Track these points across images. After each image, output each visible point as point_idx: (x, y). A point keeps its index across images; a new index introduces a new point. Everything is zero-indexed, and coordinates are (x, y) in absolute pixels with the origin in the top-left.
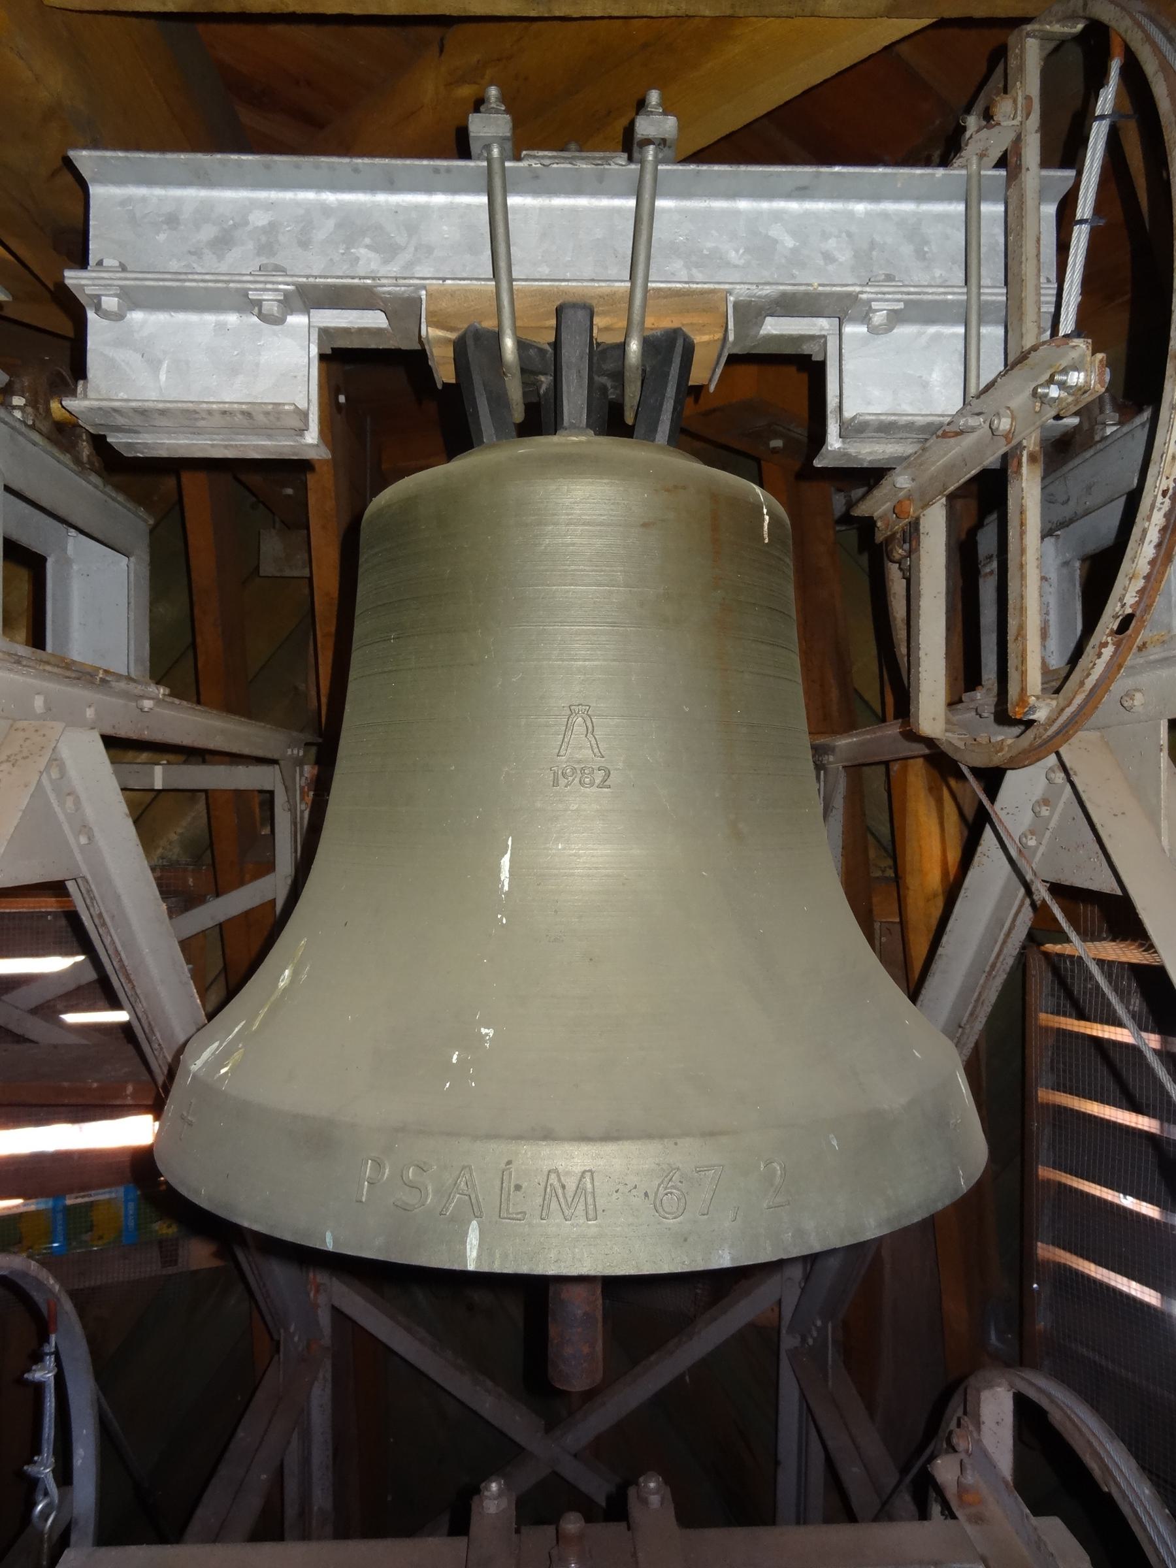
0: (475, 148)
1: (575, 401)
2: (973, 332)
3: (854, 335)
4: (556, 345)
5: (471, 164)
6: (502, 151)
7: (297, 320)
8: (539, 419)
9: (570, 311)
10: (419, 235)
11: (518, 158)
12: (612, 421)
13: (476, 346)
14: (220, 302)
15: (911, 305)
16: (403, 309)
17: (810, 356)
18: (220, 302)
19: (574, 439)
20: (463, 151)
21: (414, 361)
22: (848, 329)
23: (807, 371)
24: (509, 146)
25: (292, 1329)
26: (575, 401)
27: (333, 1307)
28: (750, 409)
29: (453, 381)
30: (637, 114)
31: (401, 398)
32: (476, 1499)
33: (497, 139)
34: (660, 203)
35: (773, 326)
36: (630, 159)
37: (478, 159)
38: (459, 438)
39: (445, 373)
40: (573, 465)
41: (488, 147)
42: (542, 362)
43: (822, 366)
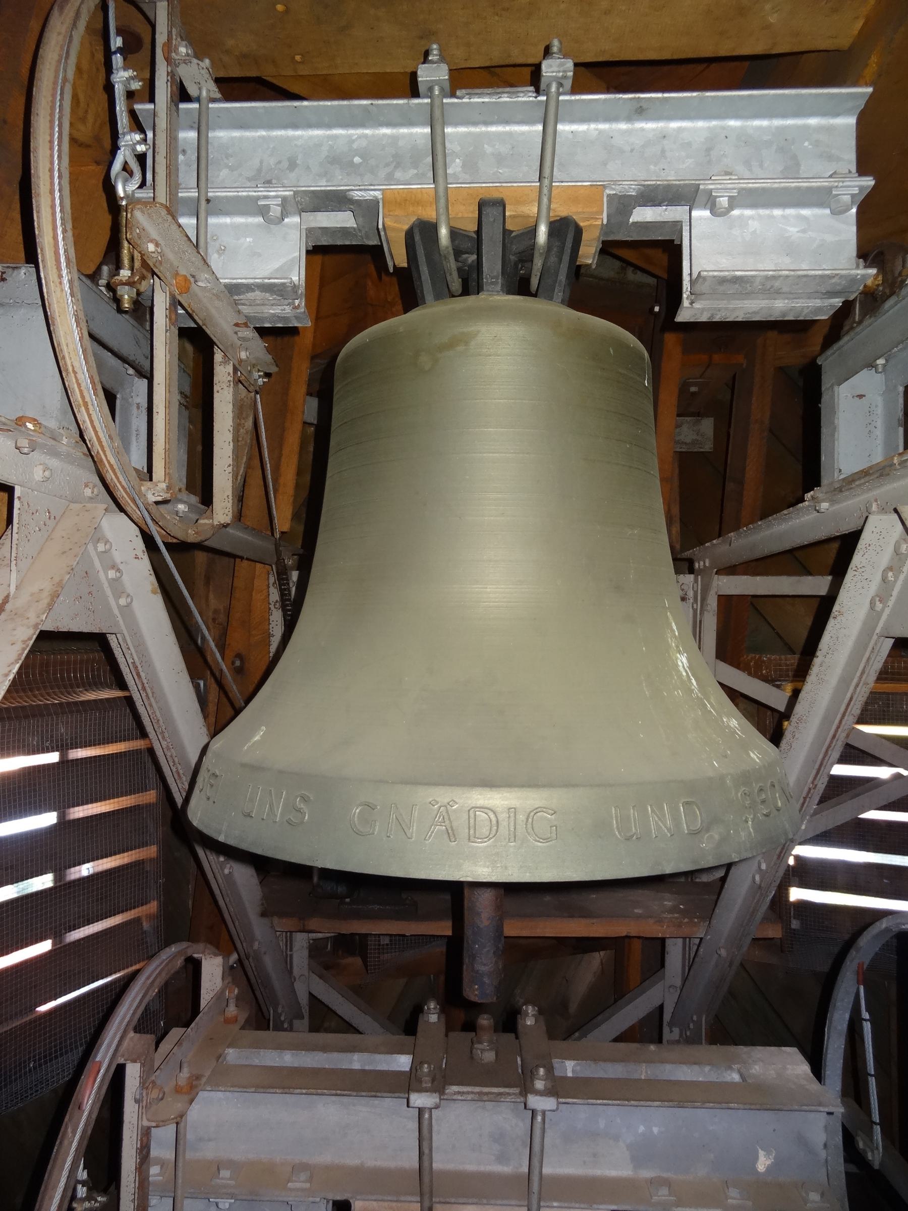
0: (422, 89)
1: (492, 265)
2: (550, 130)
3: (701, 218)
4: (479, 232)
5: (416, 101)
6: (442, 90)
7: (293, 220)
8: (471, 283)
9: (492, 206)
10: (384, 156)
11: (453, 95)
12: (520, 286)
13: (423, 232)
14: (252, 201)
15: (758, 203)
16: (368, 210)
17: (673, 241)
18: (252, 201)
19: (494, 296)
20: (415, 92)
21: (375, 253)
22: (695, 213)
23: (668, 251)
24: (447, 86)
25: (280, 1010)
26: (492, 265)
27: (310, 993)
28: (628, 278)
29: (405, 265)
30: (544, 59)
31: (365, 279)
32: (421, 1015)
33: (437, 82)
34: (560, 127)
35: (644, 214)
36: (538, 91)
37: (424, 98)
38: (410, 299)
39: (398, 256)
40: (494, 313)
41: (431, 89)
42: (469, 243)
43: (680, 247)
